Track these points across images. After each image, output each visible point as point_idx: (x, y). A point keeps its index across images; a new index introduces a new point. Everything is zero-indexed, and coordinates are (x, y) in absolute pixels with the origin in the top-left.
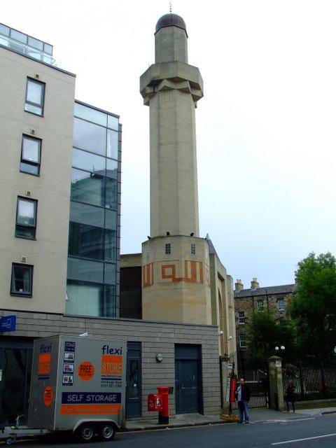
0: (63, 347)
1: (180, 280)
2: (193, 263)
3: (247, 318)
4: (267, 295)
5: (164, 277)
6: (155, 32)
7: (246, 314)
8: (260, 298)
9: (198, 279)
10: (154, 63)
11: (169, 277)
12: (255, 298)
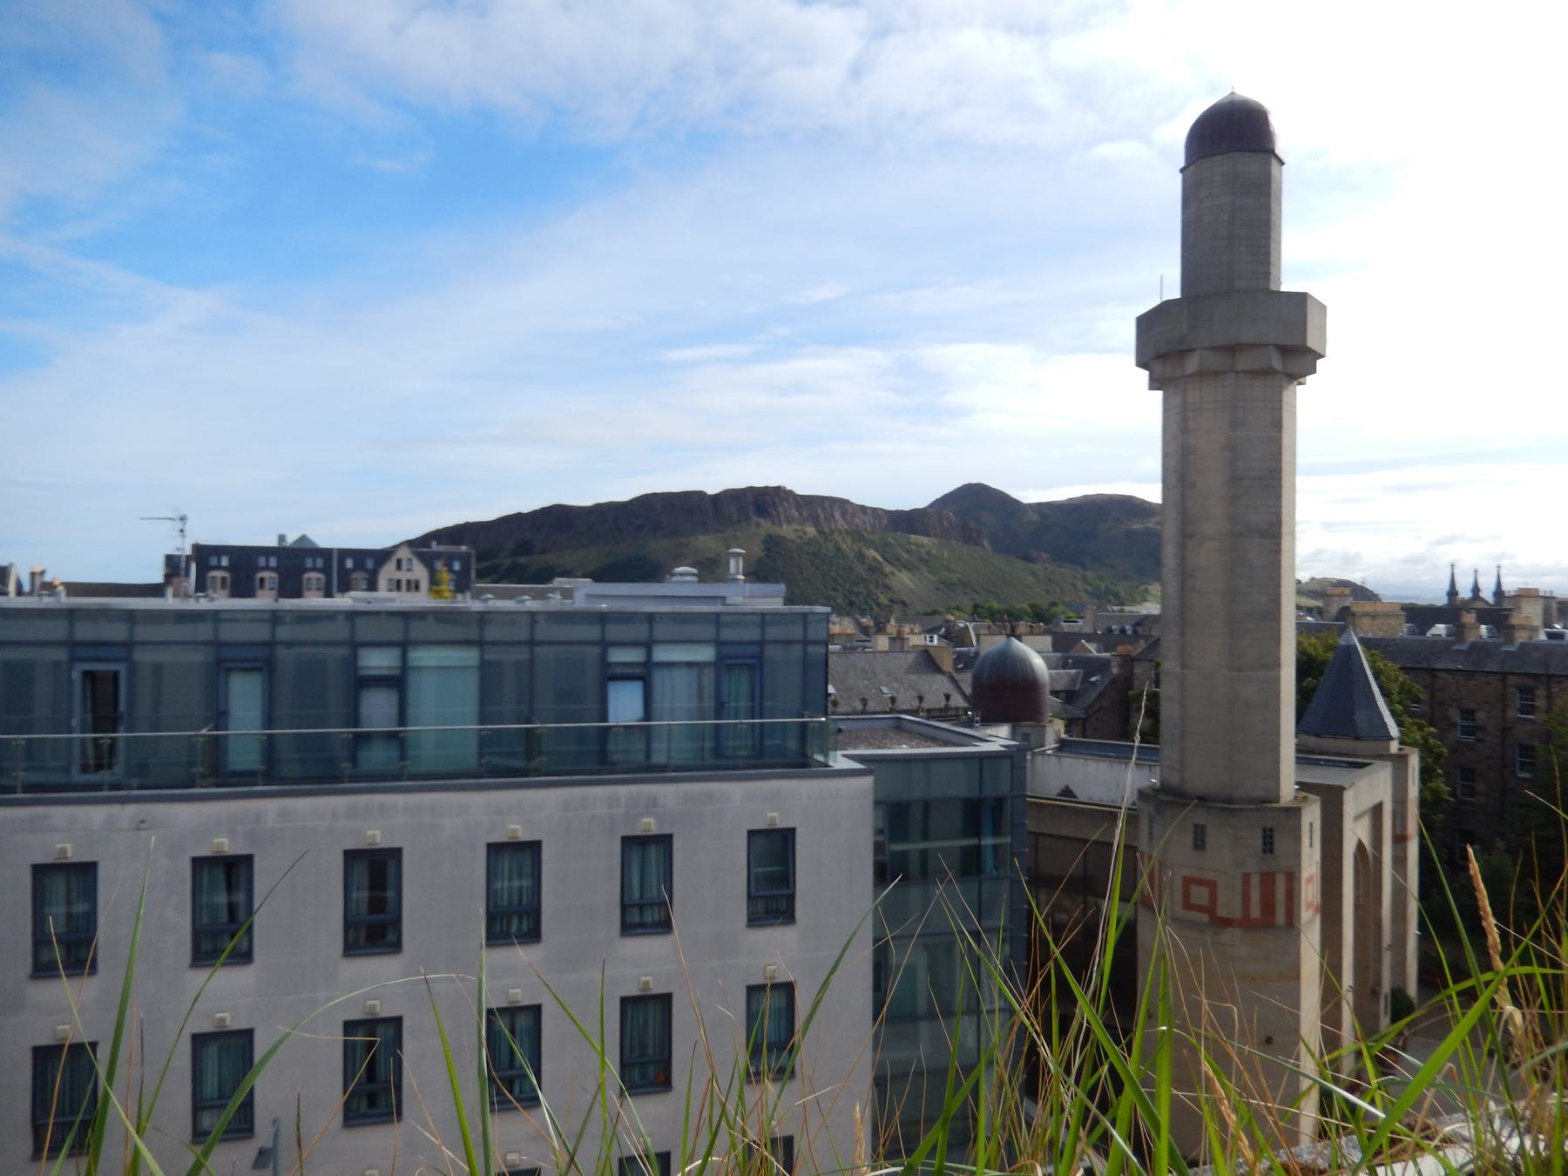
0: (376, 836)
1: (1227, 923)
2: (1268, 879)
3: (1483, 729)
4: (1550, 677)
5: (1188, 906)
6: (1182, 164)
7: (1481, 716)
8: (1528, 681)
9: (1280, 918)
10: (1174, 293)
11: (1201, 909)
12: (1512, 680)
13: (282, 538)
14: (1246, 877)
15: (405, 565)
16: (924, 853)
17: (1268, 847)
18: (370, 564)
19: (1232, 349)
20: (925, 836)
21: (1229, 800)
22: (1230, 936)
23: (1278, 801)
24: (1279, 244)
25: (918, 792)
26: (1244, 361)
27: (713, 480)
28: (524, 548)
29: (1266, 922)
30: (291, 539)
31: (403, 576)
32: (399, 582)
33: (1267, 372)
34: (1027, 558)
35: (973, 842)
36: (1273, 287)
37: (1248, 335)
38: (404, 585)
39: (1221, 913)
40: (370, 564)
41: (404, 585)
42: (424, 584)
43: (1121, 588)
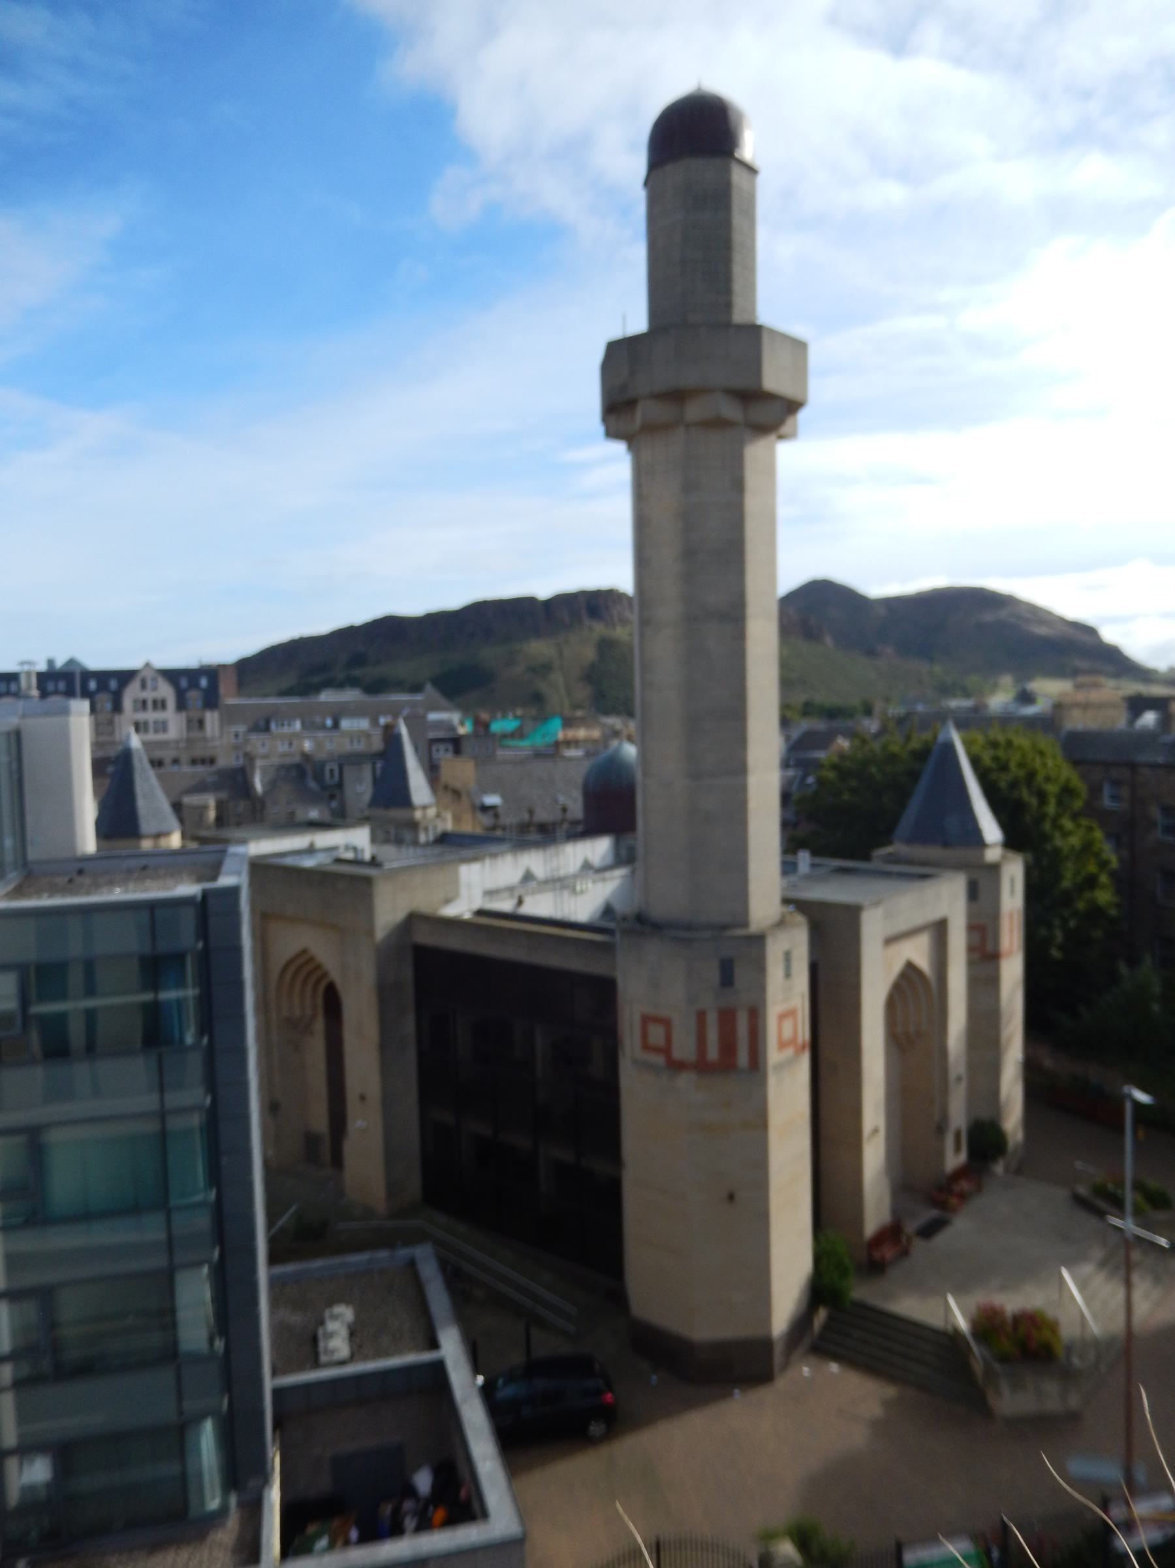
1: (675, 1066)
2: (727, 1018)
5: (646, 1047)
9: (743, 1058)
11: (657, 1050)
13: (51, 662)
14: (701, 1016)
15: (149, 683)
16: (90, 1015)
17: (727, 977)
18: (113, 684)
19: (678, 396)
20: (90, 990)
21: (689, 927)
22: (685, 1080)
23: (745, 924)
24: (750, 268)
25: (75, 949)
26: (695, 410)
27: (544, 587)
28: (358, 660)
29: (727, 1063)
30: (59, 663)
31: (149, 695)
32: (144, 702)
33: (719, 423)
34: (871, 653)
35: (148, 997)
36: (738, 317)
37: (689, 378)
38: (150, 705)
39: (677, 1054)
40: (113, 684)
41: (150, 705)
42: (171, 703)
43: (972, 680)
